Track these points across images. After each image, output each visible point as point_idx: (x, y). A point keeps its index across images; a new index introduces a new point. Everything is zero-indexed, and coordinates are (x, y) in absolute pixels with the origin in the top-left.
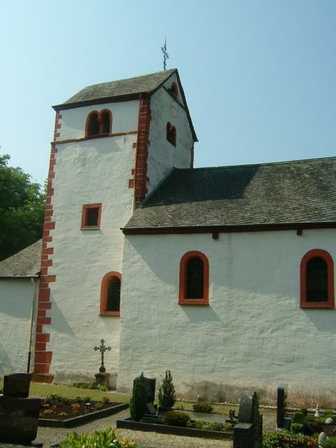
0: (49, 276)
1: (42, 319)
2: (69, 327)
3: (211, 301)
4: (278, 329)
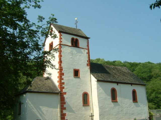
0: (63, 92)
1: (63, 108)
2: (73, 110)
3: (118, 101)
4: (130, 107)
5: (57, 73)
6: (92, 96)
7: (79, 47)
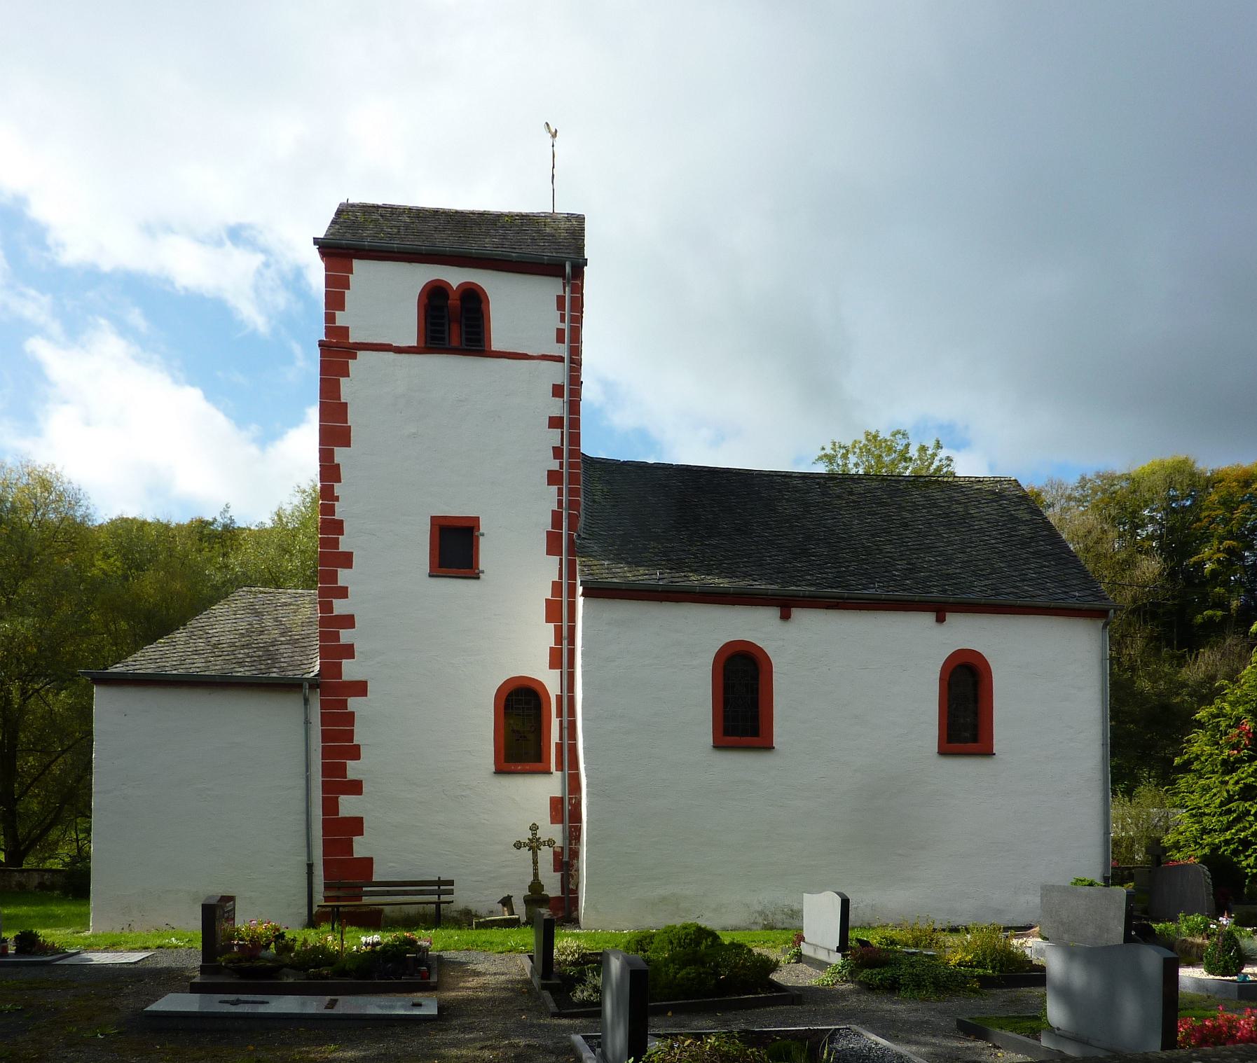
6: (756, 595)
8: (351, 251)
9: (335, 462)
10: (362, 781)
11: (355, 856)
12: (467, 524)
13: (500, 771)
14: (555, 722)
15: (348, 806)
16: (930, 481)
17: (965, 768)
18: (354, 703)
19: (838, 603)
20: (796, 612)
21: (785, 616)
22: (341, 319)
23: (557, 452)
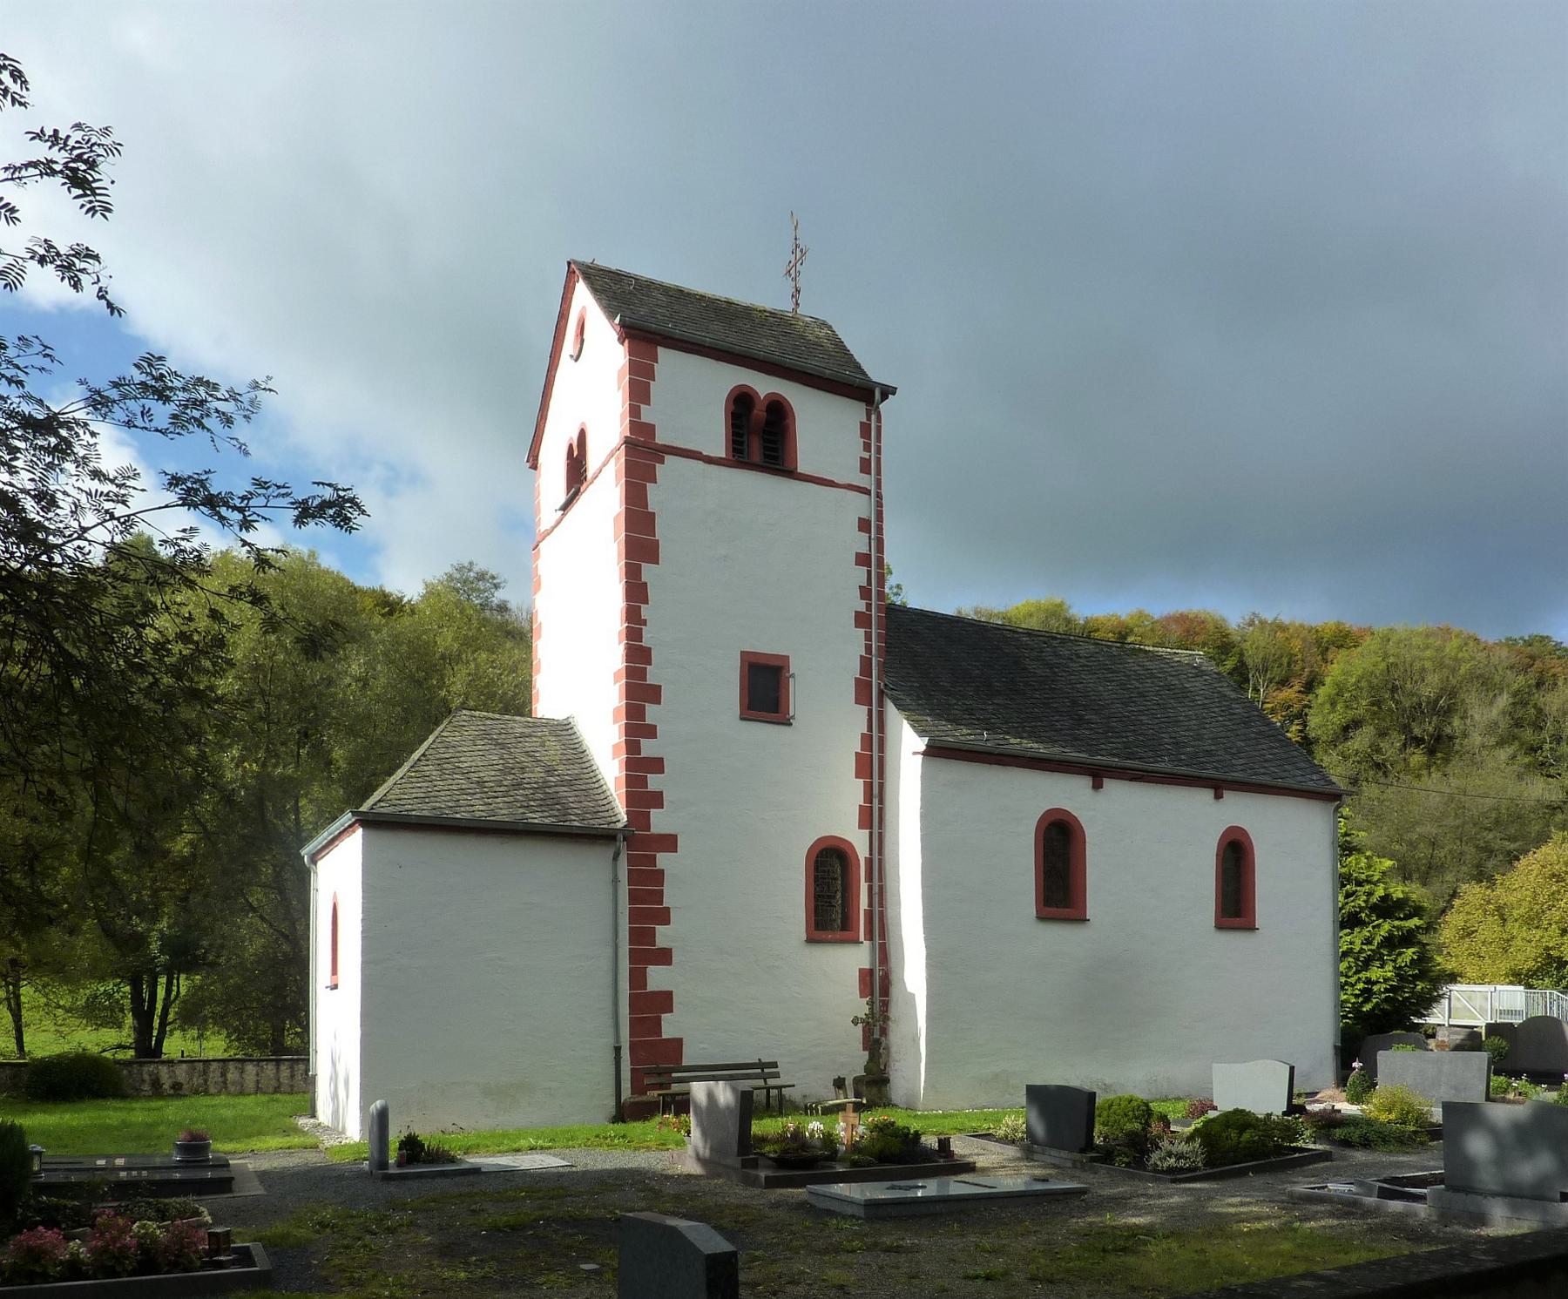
5: (610, 755)
7: (791, 473)
8: (658, 337)
9: (643, 580)
10: (671, 949)
11: (663, 1037)
12: (777, 663)
13: (811, 940)
14: (864, 887)
15: (657, 979)
16: (1134, 648)
17: (1235, 941)
18: (663, 860)
19: (1143, 776)
20: (1107, 783)
21: (1097, 786)
22: (647, 415)
23: (865, 593)
